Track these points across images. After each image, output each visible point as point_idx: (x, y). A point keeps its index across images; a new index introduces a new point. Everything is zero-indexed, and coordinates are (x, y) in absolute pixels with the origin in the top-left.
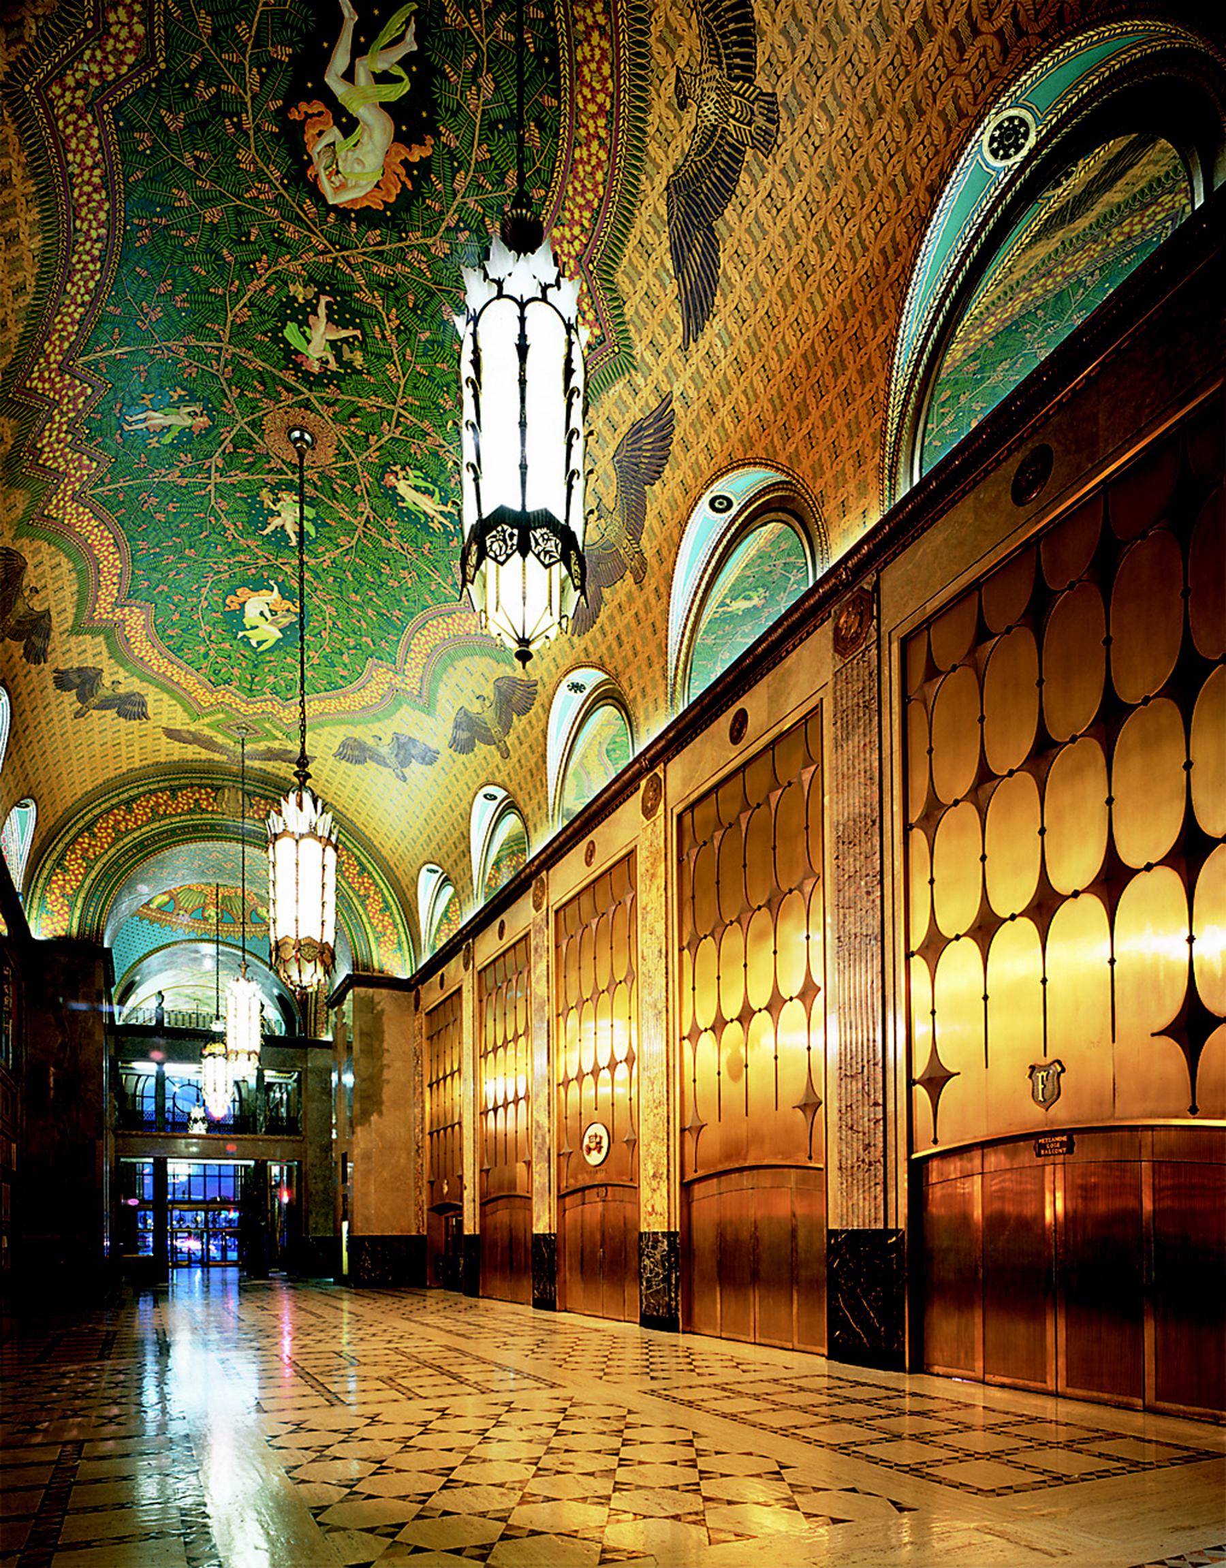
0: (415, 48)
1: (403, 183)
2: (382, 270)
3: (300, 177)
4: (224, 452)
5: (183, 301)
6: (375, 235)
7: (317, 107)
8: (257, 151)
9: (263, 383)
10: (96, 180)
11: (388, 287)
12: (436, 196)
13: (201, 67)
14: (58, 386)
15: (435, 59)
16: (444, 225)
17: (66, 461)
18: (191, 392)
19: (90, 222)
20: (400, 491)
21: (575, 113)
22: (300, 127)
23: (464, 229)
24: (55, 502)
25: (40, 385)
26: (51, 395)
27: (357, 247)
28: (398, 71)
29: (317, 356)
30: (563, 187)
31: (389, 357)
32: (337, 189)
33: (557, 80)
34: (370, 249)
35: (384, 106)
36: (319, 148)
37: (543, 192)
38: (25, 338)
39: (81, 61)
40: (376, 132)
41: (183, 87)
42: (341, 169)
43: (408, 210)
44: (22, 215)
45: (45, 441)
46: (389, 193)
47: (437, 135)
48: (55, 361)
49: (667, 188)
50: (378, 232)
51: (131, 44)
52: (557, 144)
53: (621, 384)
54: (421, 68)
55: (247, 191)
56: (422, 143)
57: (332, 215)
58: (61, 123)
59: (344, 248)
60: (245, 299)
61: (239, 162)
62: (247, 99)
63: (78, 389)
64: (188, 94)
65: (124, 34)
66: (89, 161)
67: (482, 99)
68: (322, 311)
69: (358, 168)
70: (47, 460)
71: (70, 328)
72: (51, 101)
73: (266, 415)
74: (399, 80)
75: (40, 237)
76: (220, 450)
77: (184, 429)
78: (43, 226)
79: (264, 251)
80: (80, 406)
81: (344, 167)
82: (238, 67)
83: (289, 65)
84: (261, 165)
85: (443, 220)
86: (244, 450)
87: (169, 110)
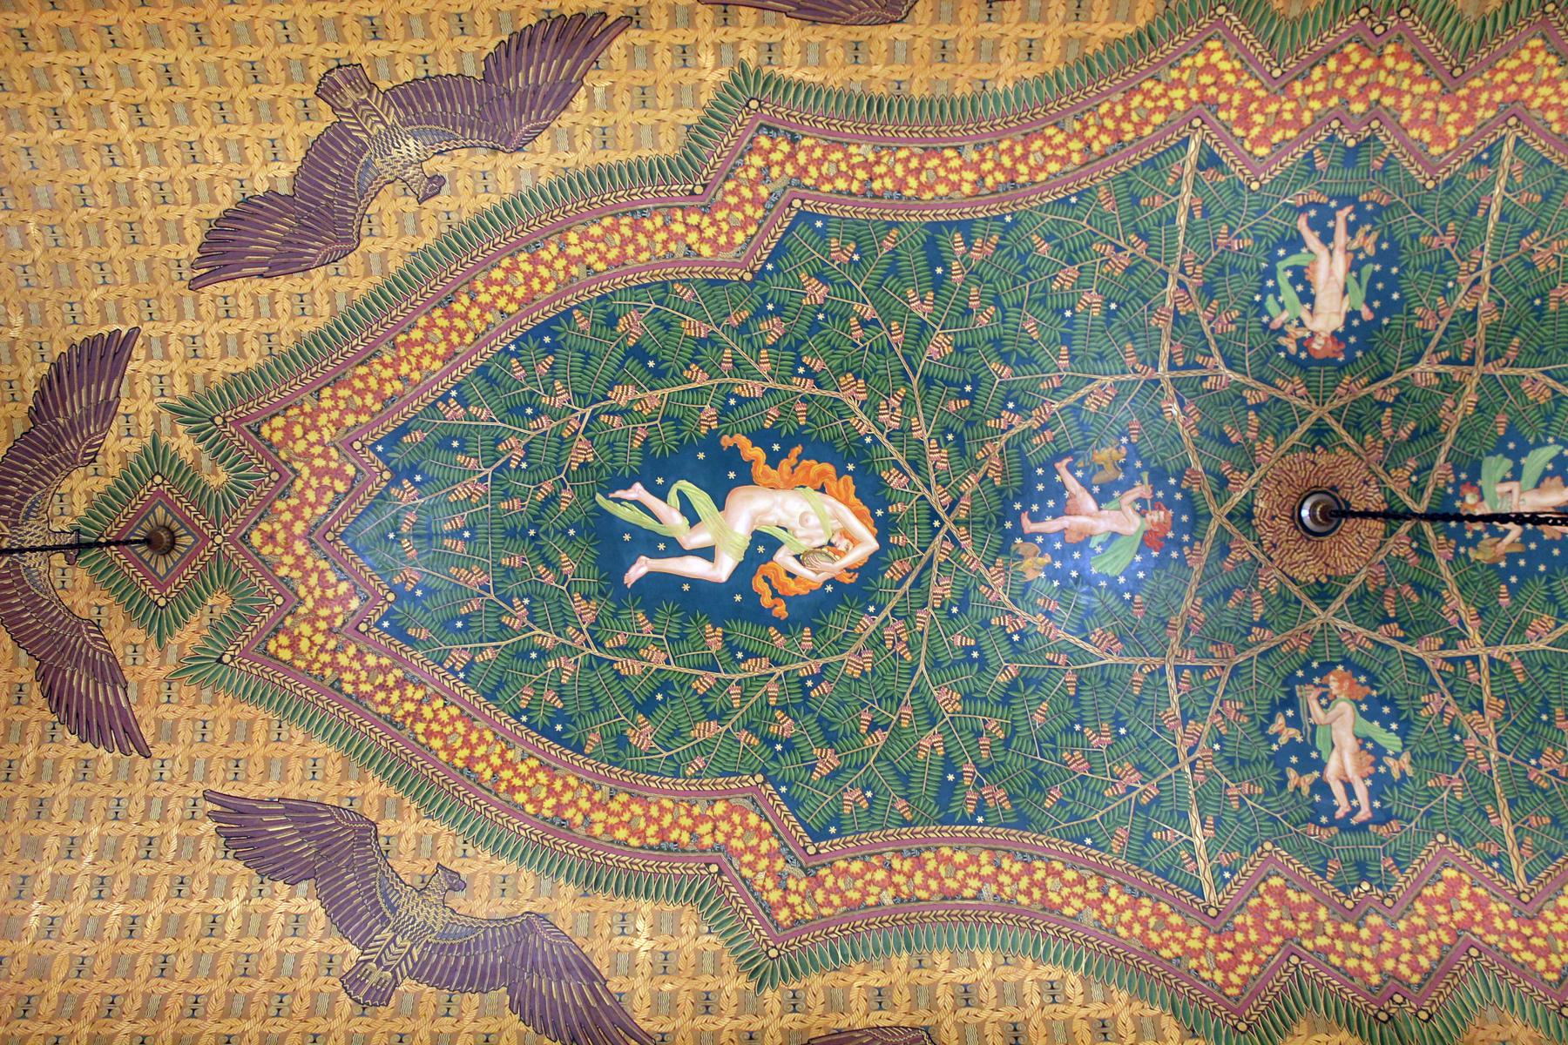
0: (638, 486)
1: (799, 458)
2: (938, 458)
3: (860, 588)
4: (1403, 640)
5: (1098, 733)
6: (895, 480)
7: (759, 584)
8: (842, 651)
9: (1227, 594)
10: (1123, 900)
11: (960, 442)
12: (786, 411)
13: (754, 731)
14: (1253, 936)
15: (636, 460)
16: (816, 392)
17: (1426, 930)
18: (1276, 707)
19: (968, 875)
20: (1337, 323)
21: (568, 285)
22: (792, 601)
23: (804, 365)
24: (1528, 956)
25: (1243, 970)
26: (1269, 949)
27: (923, 498)
28: (673, 495)
29: (1137, 520)
30: (648, 267)
31: (1075, 410)
32: (854, 541)
33: (554, 320)
34: (916, 480)
35: (721, 506)
36: (811, 575)
37: (678, 287)
38: (1141, 989)
39: (753, 881)
40: (754, 508)
41: (782, 753)
42: (824, 541)
43: (831, 444)
44: (936, 976)
45: (1368, 967)
46: (823, 474)
47: (714, 435)
48: (1203, 940)
49: (519, 149)
50: (885, 475)
51: (736, 818)
52: (613, 293)
53: (786, 72)
54: (657, 471)
55: (901, 657)
56: (735, 450)
57: (893, 539)
58: (826, 911)
59: (934, 515)
60: (1076, 640)
61: (864, 673)
62: (779, 671)
63: (1269, 901)
64: (789, 745)
65: (724, 826)
66: (880, 875)
67: (640, 395)
68: (1051, 525)
69: (813, 520)
70: (1415, 967)
71: (1144, 912)
72: (796, 922)
73: (1293, 580)
74: (680, 493)
75: (978, 953)
76: (1400, 646)
77: (1362, 714)
78: (962, 947)
79: (986, 624)
80: (1306, 898)
81: (821, 537)
82: (747, 687)
83: (725, 626)
84: (860, 644)
85: (813, 396)
86: (1387, 605)
87: (812, 768)
